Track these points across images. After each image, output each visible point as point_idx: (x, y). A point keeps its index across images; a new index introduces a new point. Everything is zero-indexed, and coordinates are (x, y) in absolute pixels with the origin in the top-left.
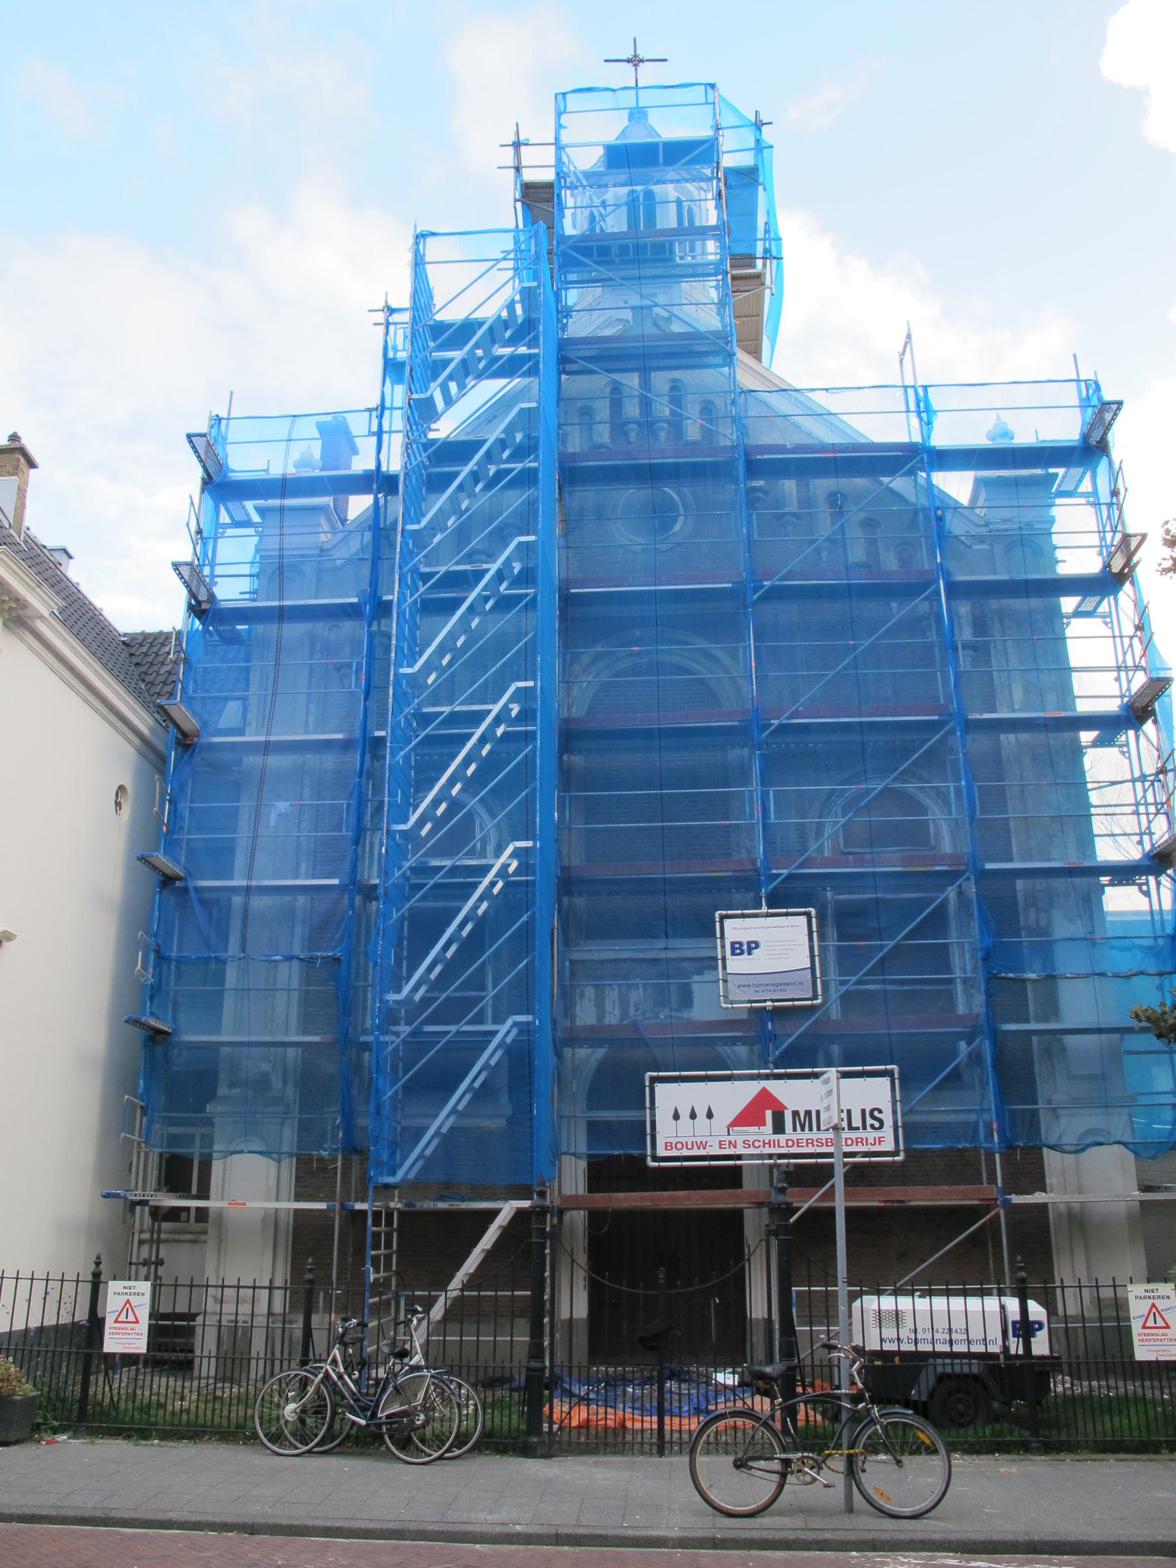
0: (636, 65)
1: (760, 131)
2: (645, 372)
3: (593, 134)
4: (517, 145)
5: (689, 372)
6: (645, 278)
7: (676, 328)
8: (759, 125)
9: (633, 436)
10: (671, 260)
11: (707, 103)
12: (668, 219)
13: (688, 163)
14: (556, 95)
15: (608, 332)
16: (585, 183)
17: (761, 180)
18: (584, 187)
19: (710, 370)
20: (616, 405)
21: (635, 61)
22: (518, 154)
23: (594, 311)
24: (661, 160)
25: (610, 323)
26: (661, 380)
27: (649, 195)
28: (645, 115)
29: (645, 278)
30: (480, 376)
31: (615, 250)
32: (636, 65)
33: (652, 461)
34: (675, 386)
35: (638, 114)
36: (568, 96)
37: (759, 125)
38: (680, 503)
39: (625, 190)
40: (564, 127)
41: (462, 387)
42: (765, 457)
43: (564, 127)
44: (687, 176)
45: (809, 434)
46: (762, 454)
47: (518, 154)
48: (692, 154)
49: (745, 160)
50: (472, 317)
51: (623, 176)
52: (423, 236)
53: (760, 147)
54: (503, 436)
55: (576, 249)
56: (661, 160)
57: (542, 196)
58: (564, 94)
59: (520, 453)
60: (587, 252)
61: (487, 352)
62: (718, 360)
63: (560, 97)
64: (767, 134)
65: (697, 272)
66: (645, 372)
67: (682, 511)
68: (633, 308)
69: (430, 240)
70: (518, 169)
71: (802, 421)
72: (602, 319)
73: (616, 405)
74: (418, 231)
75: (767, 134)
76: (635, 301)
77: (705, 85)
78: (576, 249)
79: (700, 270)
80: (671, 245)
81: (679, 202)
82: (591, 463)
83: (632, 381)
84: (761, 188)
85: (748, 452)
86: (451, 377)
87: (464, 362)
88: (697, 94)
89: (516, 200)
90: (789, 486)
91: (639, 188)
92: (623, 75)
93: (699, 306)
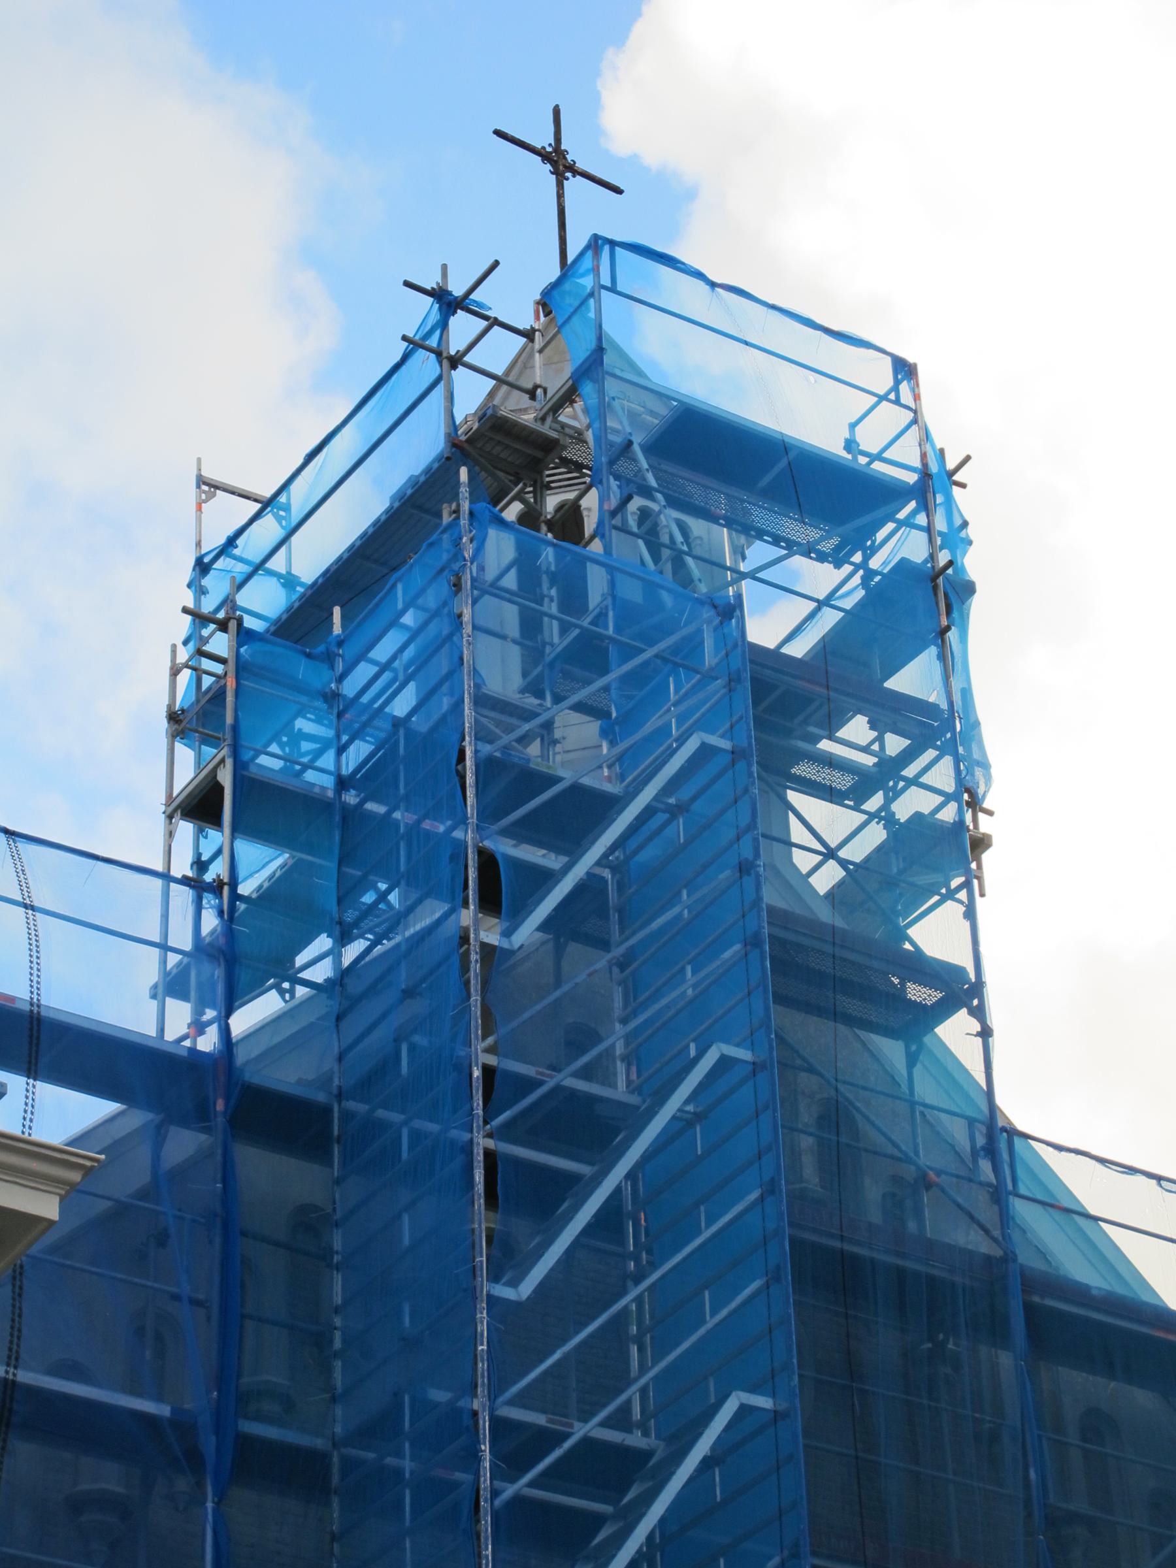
5: (813, 1021)
33: (847, 1247)
42: (1049, 1302)
58: (613, 244)
88: (882, 377)
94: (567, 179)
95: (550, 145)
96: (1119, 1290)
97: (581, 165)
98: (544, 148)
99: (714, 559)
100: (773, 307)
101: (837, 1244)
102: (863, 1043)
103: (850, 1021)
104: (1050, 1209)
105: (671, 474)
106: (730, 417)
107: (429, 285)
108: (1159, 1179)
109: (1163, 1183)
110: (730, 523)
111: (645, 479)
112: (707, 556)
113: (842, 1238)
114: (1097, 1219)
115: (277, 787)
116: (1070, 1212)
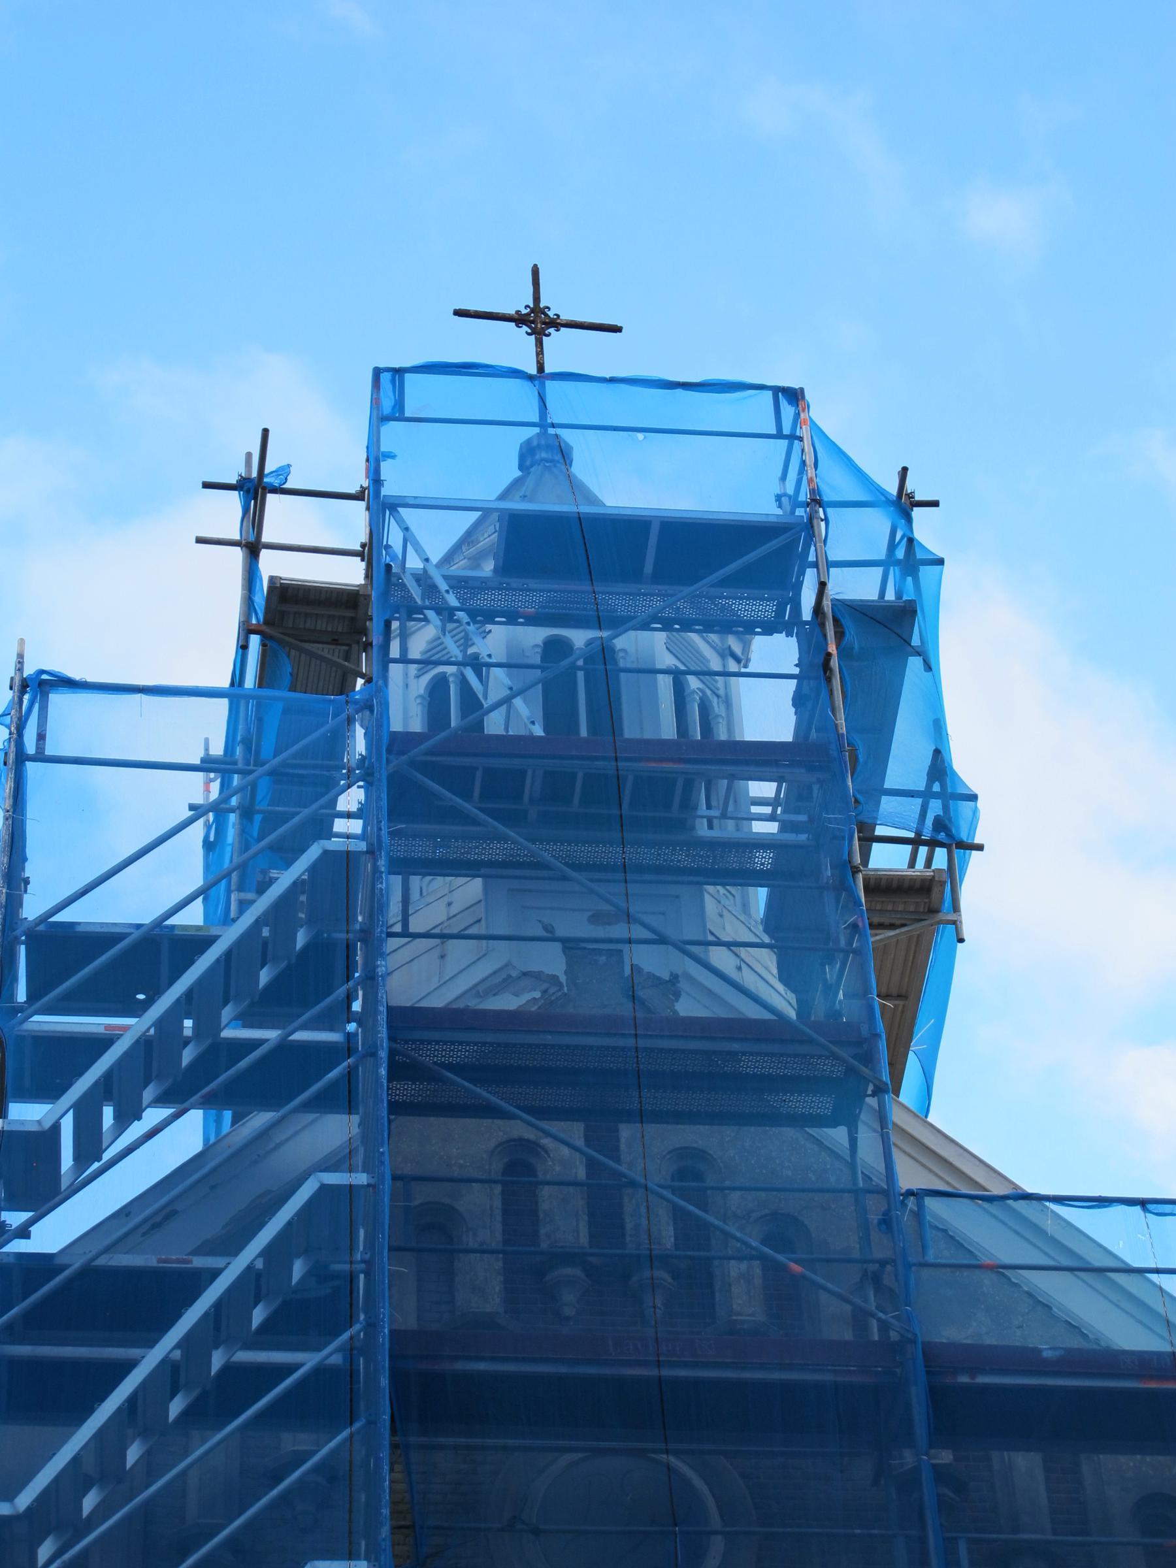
0: (539, 335)
1: (909, 519)
2: (601, 1123)
3: (460, 478)
4: (255, 490)
5: (729, 1132)
6: (641, 869)
7: (687, 1007)
8: (905, 504)
9: (569, 1299)
10: (684, 825)
11: (779, 435)
12: (655, 717)
13: (724, 583)
14: (377, 372)
15: (507, 1002)
16: (452, 600)
17: (915, 641)
18: (447, 613)
19: (789, 1132)
20: (520, 1211)
21: (537, 322)
22: (254, 518)
23: (446, 947)
24: (648, 568)
25: (504, 981)
26: (647, 1150)
27: (604, 654)
28: (564, 454)
29: (641, 869)
30: (178, 1096)
31: (533, 785)
32: (539, 335)
33: (666, 1372)
34: (690, 1169)
35: (546, 453)
36: (408, 377)
37: (905, 504)
38: (711, 1503)
39: (535, 636)
40: (390, 456)
41: (128, 1115)
42: (982, 1379)
43: (390, 456)
44: (689, 612)
45: (1074, 1328)
46: (973, 1372)
47: (254, 518)
48: (730, 565)
49: (859, 586)
50: (173, 921)
51: (536, 593)
52: (42, 684)
53: (910, 559)
54: (259, 1265)
55: (426, 768)
56: (648, 568)
57: (321, 625)
58: (399, 372)
59: (299, 1319)
60: (458, 779)
61: (208, 1026)
62: (823, 1104)
63: (385, 378)
64: (926, 528)
65: (731, 865)
66: (601, 1123)
67: (716, 1522)
68: (570, 945)
69: (58, 700)
70: (253, 549)
71: (1053, 1286)
72: (483, 970)
73: (520, 1211)
74: (28, 671)
75: (926, 528)
76: (574, 926)
77: (777, 391)
78: (426, 768)
79: (733, 861)
80: (689, 785)
81: (678, 676)
82: (482, 1366)
83: (564, 1149)
84: (914, 663)
85: (939, 1361)
86: (106, 1089)
87: (144, 1045)
88: (757, 412)
89: (246, 630)
90: (1024, 1468)
91: (579, 638)
92: (515, 349)
93: (736, 957)
94: (549, 335)
95: (527, 306)
96: (1074, 1343)
97: (565, 317)
98: (518, 312)
99: (642, 666)
100: (612, 380)
101: (653, 1372)
102: (819, 1143)
103: (773, 1119)
104: (1082, 1274)
105: (577, 592)
106: (700, 516)
107: (233, 480)
108: (1143, 1203)
109: (1150, 1206)
110: (708, 626)
111: (446, 603)
112: (634, 666)
113: (659, 1364)
114: (1141, 1271)
115: (67, 1038)
116: (1103, 1271)
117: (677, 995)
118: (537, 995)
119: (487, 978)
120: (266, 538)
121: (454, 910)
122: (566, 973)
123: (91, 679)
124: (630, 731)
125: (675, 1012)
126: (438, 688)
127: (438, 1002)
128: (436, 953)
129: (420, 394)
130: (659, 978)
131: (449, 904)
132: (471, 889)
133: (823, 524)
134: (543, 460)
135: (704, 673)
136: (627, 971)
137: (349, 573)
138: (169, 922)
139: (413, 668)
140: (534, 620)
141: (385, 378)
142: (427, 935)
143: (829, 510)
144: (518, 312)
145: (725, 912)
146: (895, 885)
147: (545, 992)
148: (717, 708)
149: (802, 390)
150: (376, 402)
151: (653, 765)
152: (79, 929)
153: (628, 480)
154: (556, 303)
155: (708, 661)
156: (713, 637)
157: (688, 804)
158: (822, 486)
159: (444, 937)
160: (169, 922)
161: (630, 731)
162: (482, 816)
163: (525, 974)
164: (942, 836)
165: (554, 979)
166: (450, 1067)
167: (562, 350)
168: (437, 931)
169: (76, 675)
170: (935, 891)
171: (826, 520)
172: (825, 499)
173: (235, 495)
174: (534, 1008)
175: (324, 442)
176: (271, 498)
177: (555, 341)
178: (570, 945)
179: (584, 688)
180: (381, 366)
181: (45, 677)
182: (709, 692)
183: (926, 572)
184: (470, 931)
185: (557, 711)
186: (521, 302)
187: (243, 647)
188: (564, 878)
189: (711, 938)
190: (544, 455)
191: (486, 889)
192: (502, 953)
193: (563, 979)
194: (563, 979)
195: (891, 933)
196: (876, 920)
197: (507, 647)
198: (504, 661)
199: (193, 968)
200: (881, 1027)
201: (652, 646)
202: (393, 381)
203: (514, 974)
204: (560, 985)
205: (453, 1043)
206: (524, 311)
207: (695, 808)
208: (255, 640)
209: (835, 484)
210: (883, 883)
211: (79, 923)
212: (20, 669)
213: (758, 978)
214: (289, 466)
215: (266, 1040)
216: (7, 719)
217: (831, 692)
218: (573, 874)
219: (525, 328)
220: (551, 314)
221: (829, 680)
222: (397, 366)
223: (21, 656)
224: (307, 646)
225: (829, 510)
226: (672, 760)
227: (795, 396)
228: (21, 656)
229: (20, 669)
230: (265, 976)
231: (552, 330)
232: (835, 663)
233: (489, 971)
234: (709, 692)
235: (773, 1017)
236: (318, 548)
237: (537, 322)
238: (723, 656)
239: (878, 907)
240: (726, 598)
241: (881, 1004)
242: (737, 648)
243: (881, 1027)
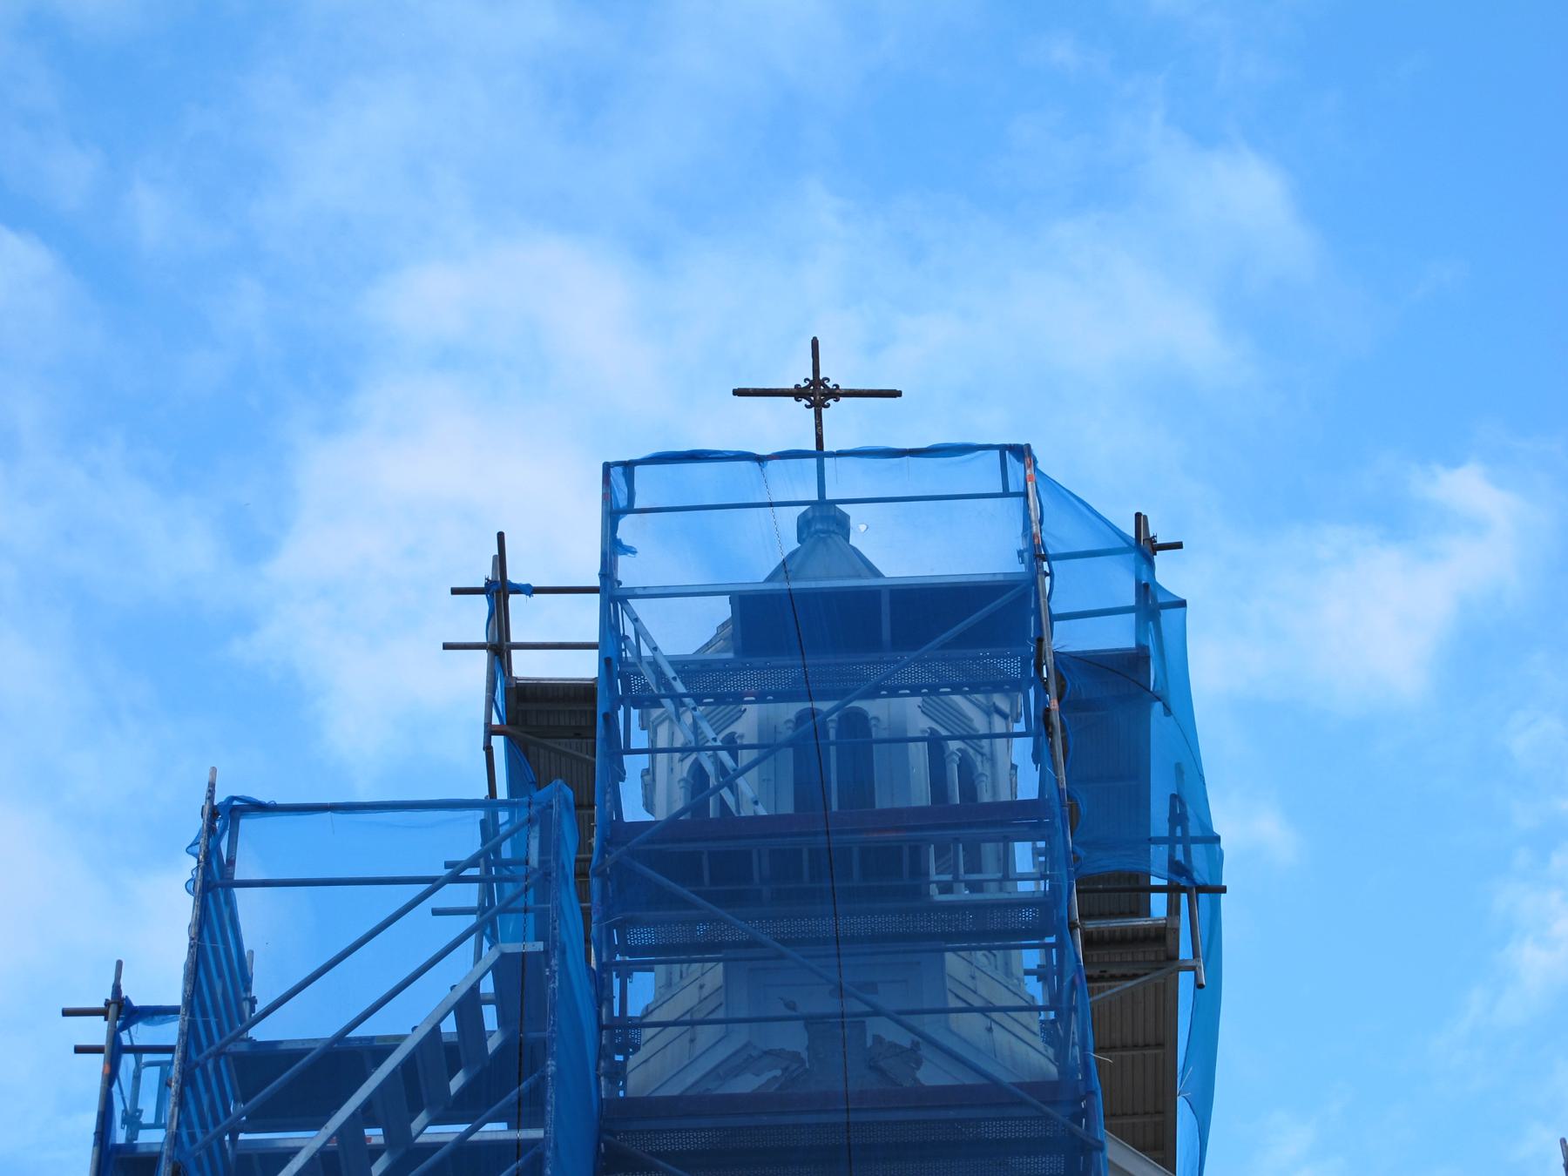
0: (818, 406)
7: (932, 1074)
8: (1145, 547)
11: (1006, 493)
14: (607, 467)
15: (746, 1084)
16: (680, 687)
18: (678, 699)
21: (817, 394)
22: (499, 618)
24: (886, 634)
27: (856, 724)
28: (843, 524)
32: (818, 406)
35: (824, 522)
37: (1145, 547)
40: (630, 550)
43: (630, 550)
47: (499, 618)
48: (976, 624)
53: (1152, 604)
56: (886, 634)
58: (628, 466)
63: (616, 473)
64: (1168, 573)
68: (810, 1021)
75: (1168, 573)
77: (1003, 449)
80: (917, 853)
81: (935, 744)
84: (1157, 707)
88: (982, 473)
89: (490, 731)
92: (788, 425)
93: (1002, 1015)
110: (973, 687)
117: (919, 1063)
118: (778, 1072)
119: (729, 1058)
120: (515, 638)
121: (706, 992)
122: (808, 1048)
123: (281, 800)
124: (882, 801)
125: (916, 1080)
126: (698, 772)
127: (673, 1090)
128: (687, 1036)
129: (650, 486)
130: (901, 1047)
131: (701, 987)
132: (714, 974)
133: (1048, 579)
134: (817, 532)
135: (971, 737)
136: (869, 1043)
137: (584, 667)
138: (351, 1035)
139: (677, 756)
140: (780, 697)
141: (616, 473)
142: (675, 1023)
143: (1053, 563)
144: (797, 386)
145: (978, 974)
146: (1141, 934)
147: (785, 1069)
148: (981, 767)
149: (1028, 446)
150: (608, 496)
151: (864, 836)
152: (283, 1047)
153: (900, 547)
154: (835, 373)
155: (971, 720)
156: (979, 697)
157: (919, 871)
158: (1047, 539)
159: (693, 1023)
160: (351, 1035)
161: (882, 801)
162: (700, 901)
163: (765, 1053)
164: (1183, 882)
165: (796, 1056)
166: (658, 1155)
167: (846, 425)
168: (688, 1017)
169: (265, 798)
170: (1169, 938)
171: (1051, 574)
172: (1050, 552)
173: (483, 597)
174: (772, 1089)
175: (559, 541)
176: (512, 598)
177: (834, 411)
178: (810, 1021)
179: (832, 757)
180: (611, 460)
181: (236, 803)
182: (971, 752)
183: (1167, 616)
184: (712, 1017)
185: (810, 788)
186: (799, 375)
187: (488, 749)
188: (781, 957)
189: (953, 1003)
190: (819, 526)
191: (727, 974)
192: (741, 1035)
193: (805, 1055)
194: (805, 1055)
195: (1129, 984)
196: (1095, 972)
197: (760, 725)
198: (755, 741)
199: (364, 1086)
200: (1096, 1084)
201: (907, 713)
202: (624, 474)
203: (755, 1053)
204: (802, 1062)
205: (679, 1131)
206: (803, 385)
207: (927, 874)
208: (498, 742)
209: (1061, 533)
210: (1141, 934)
211: (281, 1042)
212: (211, 797)
213: (1013, 1039)
214: (634, 552)
215: (444, 1143)
216: (196, 849)
217: (1052, 746)
218: (787, 950)
219: (805, 402)
220: (830, 385)
221: (1050, 734)
222: (626, 459)
223: (212, 786)
224: (548, 742)
225: (1053, 563)
226: (897, 830)
227: (1022, 452)
228: (212, 786)
229: (211, 797)
230: (456, 1083)
231: (831, 401)
232: (1055, 719)
233: (730, 1051)
234: (971, 752)
235: (986, 1082)
236: (559, 644)
237: (817, 394)
238: (988, 714)
239: (1118, 959)
240: (991, 657)
241: (1098, 1061)
242: (1004, 705)
243: (1096, 1084)
